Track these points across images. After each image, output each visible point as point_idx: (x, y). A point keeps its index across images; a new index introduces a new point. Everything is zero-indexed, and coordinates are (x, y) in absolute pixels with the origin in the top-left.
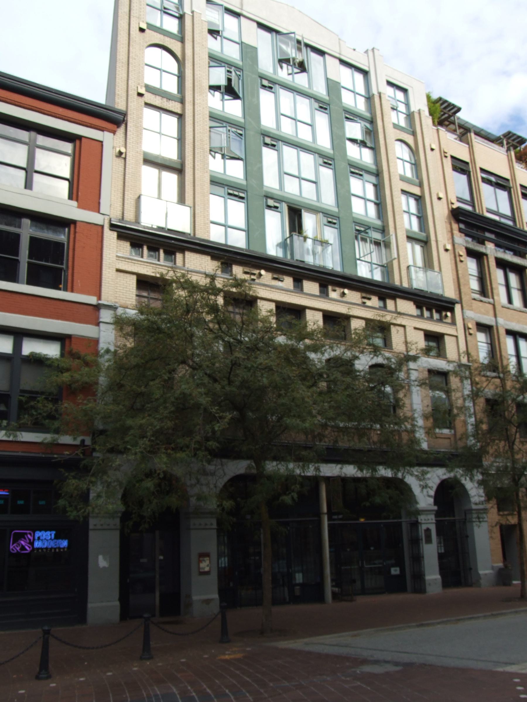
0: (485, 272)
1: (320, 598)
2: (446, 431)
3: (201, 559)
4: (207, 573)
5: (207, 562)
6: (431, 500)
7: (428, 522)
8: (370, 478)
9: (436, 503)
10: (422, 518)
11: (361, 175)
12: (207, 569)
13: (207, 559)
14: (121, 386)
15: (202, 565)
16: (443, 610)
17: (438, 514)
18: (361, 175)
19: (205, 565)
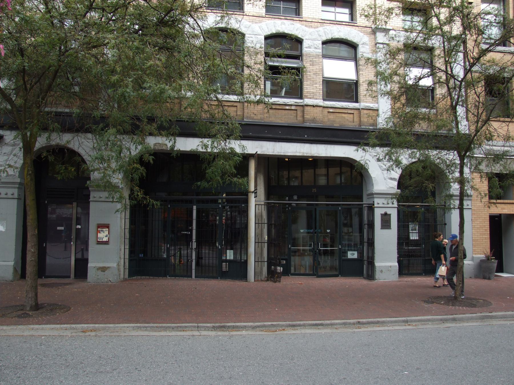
0: (288, 4)
1: (243, 275)
2: (233, 98)
3: (99, 229)
4: (106, 243)
5: (106, 233)
6: (395, 183)
7: (385, 207)
8: (402, 172)
9: (400, 185)
10: (378, 202)
11: (23, 276)
12: (105, 239)
13: (106, 230)
14: (211, 156)
15: (100, 235)
16: (391, 303)
17: (400, 199)
18: (23, 276)
19: (103, 235)
